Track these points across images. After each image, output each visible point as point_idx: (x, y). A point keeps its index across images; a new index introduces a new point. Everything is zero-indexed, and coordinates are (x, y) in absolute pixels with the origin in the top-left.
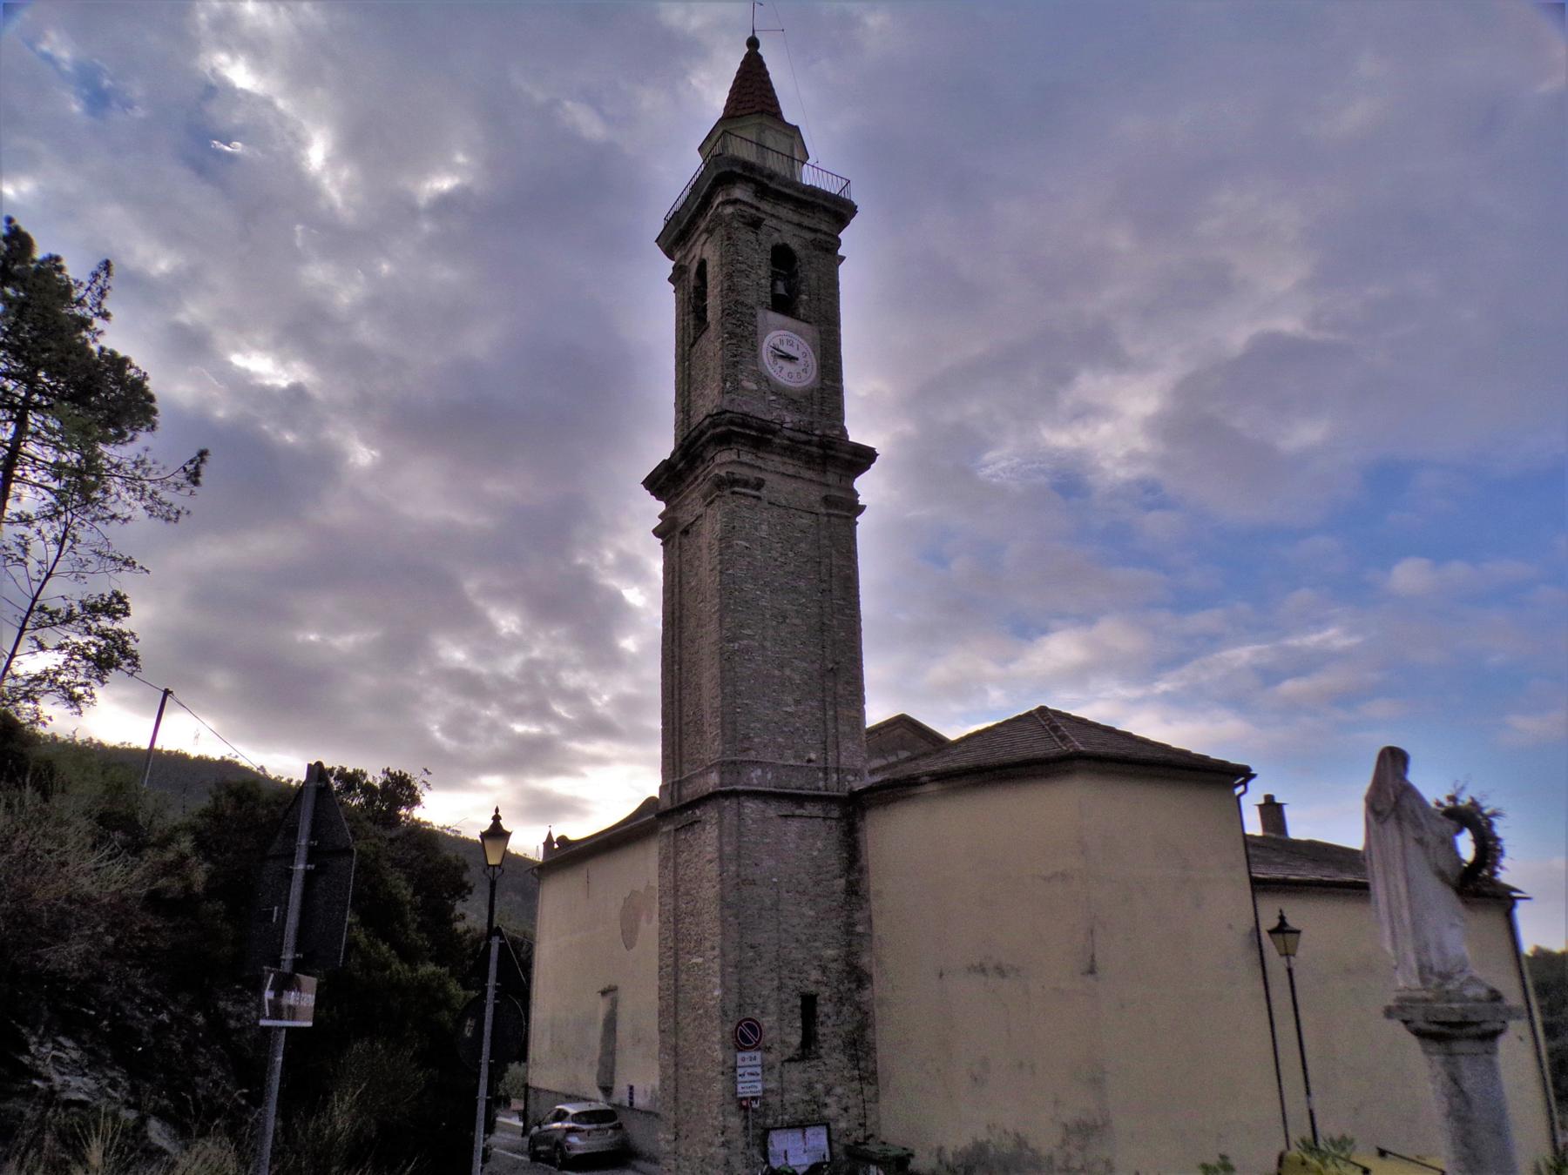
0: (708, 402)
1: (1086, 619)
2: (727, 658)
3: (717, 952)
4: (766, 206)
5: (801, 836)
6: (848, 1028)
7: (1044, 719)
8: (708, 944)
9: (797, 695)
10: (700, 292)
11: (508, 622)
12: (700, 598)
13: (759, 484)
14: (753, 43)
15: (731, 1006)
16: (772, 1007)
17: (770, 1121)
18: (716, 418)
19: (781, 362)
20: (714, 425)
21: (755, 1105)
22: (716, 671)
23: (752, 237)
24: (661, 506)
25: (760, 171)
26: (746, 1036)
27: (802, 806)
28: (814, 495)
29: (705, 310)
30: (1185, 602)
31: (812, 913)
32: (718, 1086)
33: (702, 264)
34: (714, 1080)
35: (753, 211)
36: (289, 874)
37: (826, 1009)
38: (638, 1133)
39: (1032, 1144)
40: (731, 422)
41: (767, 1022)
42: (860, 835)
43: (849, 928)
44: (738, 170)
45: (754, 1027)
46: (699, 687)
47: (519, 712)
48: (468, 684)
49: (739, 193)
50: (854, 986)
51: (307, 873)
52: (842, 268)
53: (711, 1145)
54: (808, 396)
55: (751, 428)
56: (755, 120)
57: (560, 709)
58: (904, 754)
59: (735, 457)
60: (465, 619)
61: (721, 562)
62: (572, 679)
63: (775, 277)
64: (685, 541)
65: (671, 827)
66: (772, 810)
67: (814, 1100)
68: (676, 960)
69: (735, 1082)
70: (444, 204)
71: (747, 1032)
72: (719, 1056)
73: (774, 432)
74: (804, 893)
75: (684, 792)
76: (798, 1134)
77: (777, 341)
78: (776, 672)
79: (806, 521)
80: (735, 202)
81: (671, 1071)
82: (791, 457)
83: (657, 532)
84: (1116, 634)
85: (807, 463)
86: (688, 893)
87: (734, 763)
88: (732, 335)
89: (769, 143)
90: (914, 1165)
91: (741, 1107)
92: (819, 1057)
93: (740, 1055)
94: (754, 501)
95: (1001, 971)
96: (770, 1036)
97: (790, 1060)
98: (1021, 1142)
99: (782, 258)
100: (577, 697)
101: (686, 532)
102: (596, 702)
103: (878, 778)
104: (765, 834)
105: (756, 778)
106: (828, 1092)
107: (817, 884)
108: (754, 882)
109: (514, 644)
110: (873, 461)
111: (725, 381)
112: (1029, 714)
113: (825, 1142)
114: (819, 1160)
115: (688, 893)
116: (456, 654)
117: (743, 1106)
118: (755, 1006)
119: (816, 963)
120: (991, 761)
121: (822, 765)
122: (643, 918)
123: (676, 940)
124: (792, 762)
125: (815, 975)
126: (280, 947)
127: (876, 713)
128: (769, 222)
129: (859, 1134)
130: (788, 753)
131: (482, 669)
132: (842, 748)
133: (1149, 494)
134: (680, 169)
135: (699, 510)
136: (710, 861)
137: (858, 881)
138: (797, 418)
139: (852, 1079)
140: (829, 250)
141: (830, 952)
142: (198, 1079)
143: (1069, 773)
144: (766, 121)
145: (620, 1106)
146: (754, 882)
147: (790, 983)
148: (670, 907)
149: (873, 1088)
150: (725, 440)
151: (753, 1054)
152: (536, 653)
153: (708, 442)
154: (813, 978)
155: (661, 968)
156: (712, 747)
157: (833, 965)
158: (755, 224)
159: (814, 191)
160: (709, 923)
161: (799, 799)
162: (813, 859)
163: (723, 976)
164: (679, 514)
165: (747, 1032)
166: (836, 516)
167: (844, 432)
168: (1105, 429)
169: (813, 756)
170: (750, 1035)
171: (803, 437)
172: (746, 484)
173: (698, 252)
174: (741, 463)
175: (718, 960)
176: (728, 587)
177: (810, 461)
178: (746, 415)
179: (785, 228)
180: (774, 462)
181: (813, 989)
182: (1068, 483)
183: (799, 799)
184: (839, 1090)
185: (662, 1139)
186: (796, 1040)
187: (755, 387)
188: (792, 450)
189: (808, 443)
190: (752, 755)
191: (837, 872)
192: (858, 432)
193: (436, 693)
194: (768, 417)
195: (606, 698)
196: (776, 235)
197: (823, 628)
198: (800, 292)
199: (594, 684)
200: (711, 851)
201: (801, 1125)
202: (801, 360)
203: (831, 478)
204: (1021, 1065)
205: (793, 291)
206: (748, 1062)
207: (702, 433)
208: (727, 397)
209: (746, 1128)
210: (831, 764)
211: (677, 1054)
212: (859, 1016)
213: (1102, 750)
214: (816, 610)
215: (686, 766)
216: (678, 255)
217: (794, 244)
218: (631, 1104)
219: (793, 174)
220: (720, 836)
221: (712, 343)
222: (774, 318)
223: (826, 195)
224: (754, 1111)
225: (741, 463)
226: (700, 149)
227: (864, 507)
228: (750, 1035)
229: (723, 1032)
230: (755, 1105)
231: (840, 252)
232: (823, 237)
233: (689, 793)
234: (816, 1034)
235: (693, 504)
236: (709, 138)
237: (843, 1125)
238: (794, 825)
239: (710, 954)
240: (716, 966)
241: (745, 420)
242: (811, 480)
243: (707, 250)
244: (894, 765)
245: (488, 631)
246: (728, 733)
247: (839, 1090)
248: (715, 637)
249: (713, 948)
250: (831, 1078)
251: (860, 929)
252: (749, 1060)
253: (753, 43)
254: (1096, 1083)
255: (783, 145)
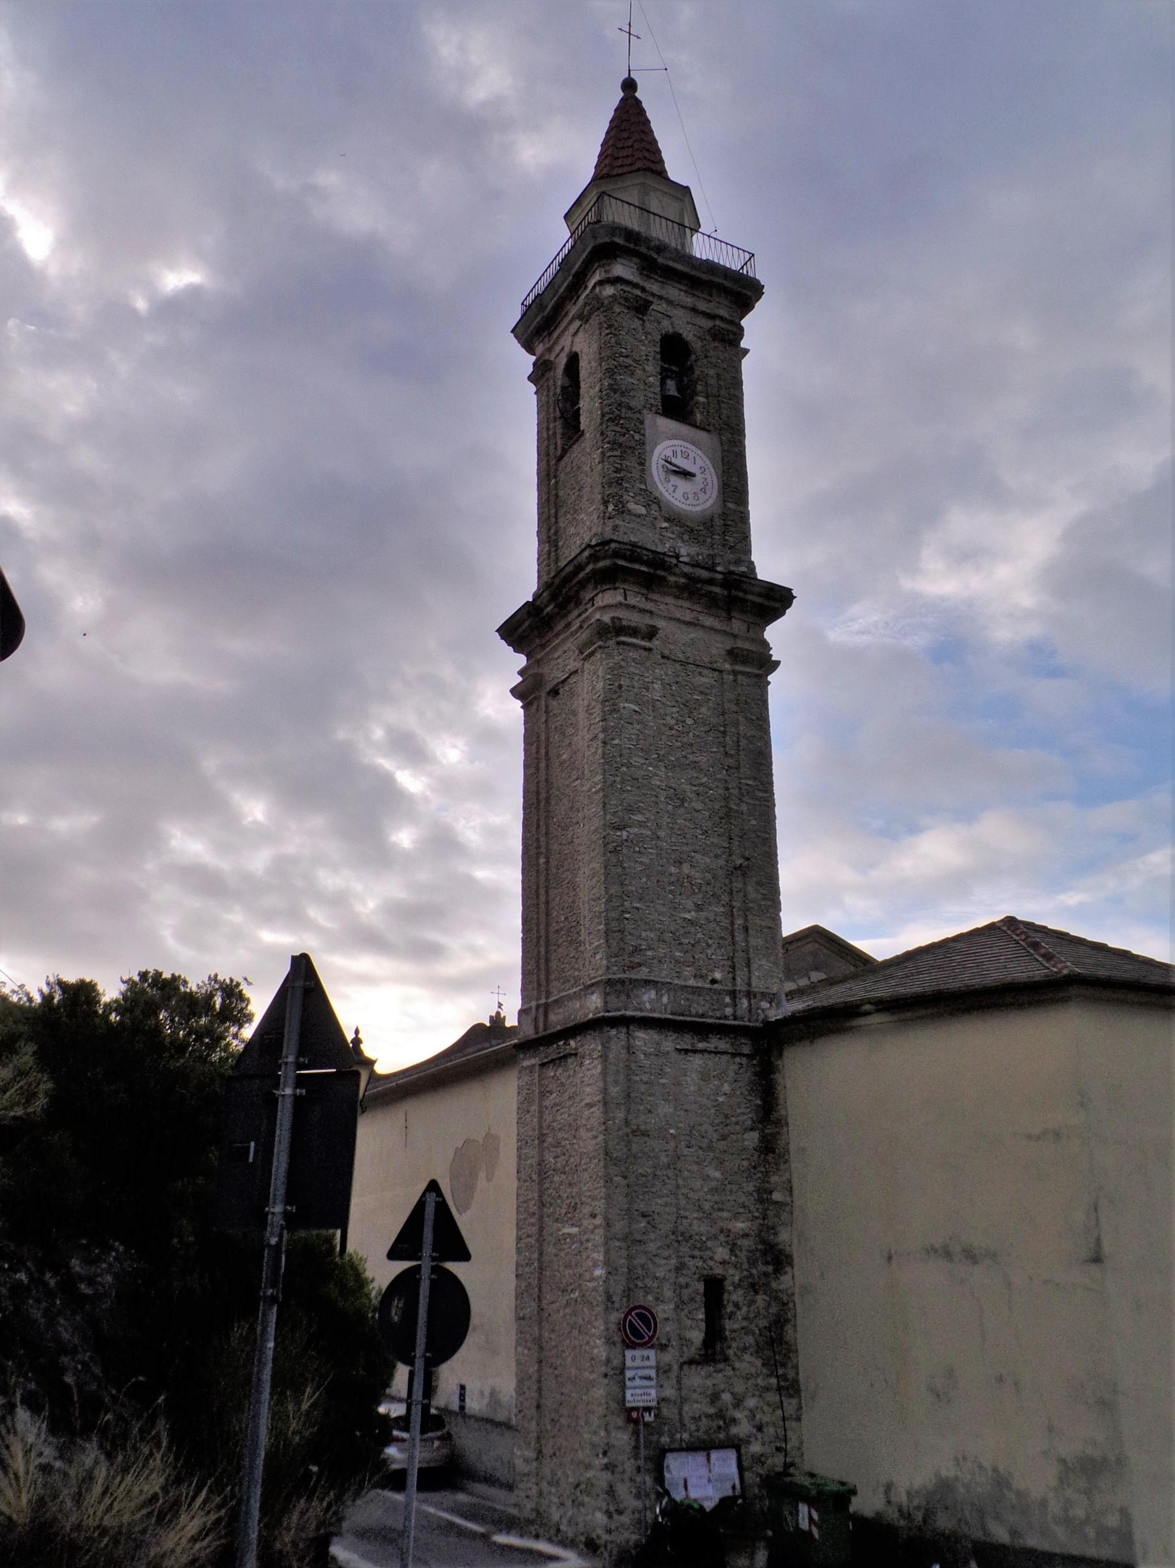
0: (585, 528)
1: (966, 814)
2: (613, 850)
3: (599, 1221)
4: (654, 287)
5: (705, 1077)
6: (764, 1323)
7: (1011, 930)
8: (586, 1210)
9: (698, 898)
10: (571, 392)
11: (255, 809)
12: (574, 775)
13: (652, 633)
14: (629, 85)
15: (617, 1289)
16: (668, 1293)
17: (665, 1440)
18: (599, 549)
19: (675, 480)
20: (594, 558)
21: (649, 1418)
22: (597, 865)
23: (637, 323)
24: (521, 660)
25: (647, 240)
26: (637, 1329)
27: (705, 1038)
28: (718, 646)
29: (577, 414)
30: (1094, 792)
31: (717, 1174)
32: (599, 1393)
33: (574, 359)
34: (592, 1384)
35: (638, 292)
36: (272, 1103)
37: (734, 1297)
38: (469, 1441)
39: (1019, 1483)
40: (616, 554)
41: (663, 1311)
42: (777, 1077)
43: (763, 1196)
44: (620, 241)
45: (648, 1317)
46: (573, 886)
47: (269, 917)
48: (205, 882)
49: (620, 269)
50: (770, 1268)
51: (297, 1099)
52: (746, 363)
53: (588, 1467)
54: (708, 523)
55: (639, 560)
56: (638, 179)
57: (314, 913)
58: (816, 976)
59: (620, 598)
60: (205, 804)
61: (604, 730)
62: (329, 880)
63: (664, 375)
64: (554, 703)
65: (534, 1061)
66: (669, 1043)
67: (720, 1415)
68: (541, 1229)
69: (623, 1387)
70: (173, 309)
71: (638, 1324)
72: (600, 1351)
73: (668, 569)
74: (710, 1148)
75: (553, 1017)
76: (700, 1457)
77: (669, 453)
78: (673, 869)
79: (706, 679)
80: (618, 280)
81: (533, 1369)
82: (690, 598)
83: (516, 692)
84: (998, 830)
85: (708, 607)
86: (558, 1145)
87: (622, 982)
88: (615, 444)
89: (654, 206)
90: (857, 1505)
91: (629, 1420)
92: (726, 1359)
93: (629, 1354)
94: (645, 654)
95: (971, 1256)
96: (666, 1330)
97: (691, 1362)
98: (1001, 1482)
99: (674, 351)
100: (339, 901)
101: (554, 692)
102: (359, 908)
103: (797, 1006)
104: (661, 1073)
105: (649, 1002)
106: (738, 1403)
107: (724, 1138)
108: (645, 1134)
109: (263, 835)
110: (789, 605)
111: (605, 503)
112: (991, 927)
113: (734, 1469)
114: (730, 1493)
115: (558, 1145)
116: (188, 843)
117: (631, 1417)
118: (647, 1290)
119: (722, 1238)
120: (954, 985)
121: (729, 987)
122: (482, 1175)
123: (542, 1205)
124: (692, 982)
125: (722, 1253)
126: (265, 1199)
127: (792, 923)
128: (658, 306)
129: (777, 1461)
130: (688, 971)
131: (224, 865)
132: (754, 966)
133: (1040, 659)
134: (544, 242)
135: (573, 665)
136: (590, 1105)
137: (775, 1136)
138: (694, 550)
139: (767, 1389)
140: (730, 339)
141: (740, 1225)
142: (65, 1360)
143: (1065, 1000)
144: (651, 181)
145: (446, 1410)
146: (645, 1134)
147: (691, 1263)
148: (534, 1161)
149: (794, 1401)
150: (608, 578)
151: (646, 1352)
152: (290, 849)
153: (587, 580)
154: (718, 1257)
155: (519, 1239)
156: (594, 960)
157: (745, 1243)
158: (641, 308)
159: (711, 267)
160: (590, 1185)
161: (701, 1030)
162: (718, 1105)
163: (607, 1252)
164: (545, 670)
165: (638, 1324)
166: (743, 673)
167: (751, 566)
168: (1003, 572)
169: (718, 975)
170: (642, 1328)
171: (704, 574)
172: (634, 632)
173: (568, 343)
174: (628, 606)
175: (601, 1231)
176: (612, 763)
177: (711, 603)
178: (634, 545)
179: (677, 313)
180: (668, 604)
181: (718, 1271)
182: (952, 644)
183: (701, 1030)
184: (751, 1402)
185: (516, 1454)
186: (697, 1336)
187: (643, 511)
188: (692, 589)
189: (711, 582)
190: (643, 973)
191: (749, 1123)
192: (769, 563)
193: (169, 892)
194: (660, 549)
195: (371, 904)
196: (666, 323)
197: (728, 815)
198: (695, 393)
199: (358, 887)
200: (591, 1093)
201: (703, 1446)
202: (699, 477)
203: (737, 626)
204: (1000, 1379)
205: (687, 390)
206: (638, 1363)
207: (580, 568)
208: (610, 523)
209: (636, 1448)
210: (740, 985)
211: (541, 1348)
212: (774, 1310)
213: (1102, 973)
214: (721, 791)
215: (555, 985)
216: (540, 348)
217: (688, 334)
218: (462, 1408)
219: (683, 245)
220: (604, 1073)
221: (588, 456)
222: (665, 424)
223: (726, 272)
224: (646, 1425)
225: (628, 606)
226: (567, 217)
227: (777, 663)
228: (642, 1328)
229: (606, 1323)
230: (649, 1418)
231: (743, 344)
232: (723, 325)
233: (557, 1020)
234: (723, 1329)
235: (564, 656)
236: (578, 203)
237: (756, 1448)
238: (697, 1061)
239: (587, 1223)
240: (598, 1237)
241: (633, 552)
242: (712, 629)
243: (580, 341)
244: (813, 988)
245: (229, 818)
246: (614, 944)
247: (751, 1402)
248: (597, 823)
249: (594, 1216)
250: (739, 1388)
251: (776, 1196)
252: (640, 1360)
253: (629, 85)
254: (1106, 1406)
255: (672, 211)
